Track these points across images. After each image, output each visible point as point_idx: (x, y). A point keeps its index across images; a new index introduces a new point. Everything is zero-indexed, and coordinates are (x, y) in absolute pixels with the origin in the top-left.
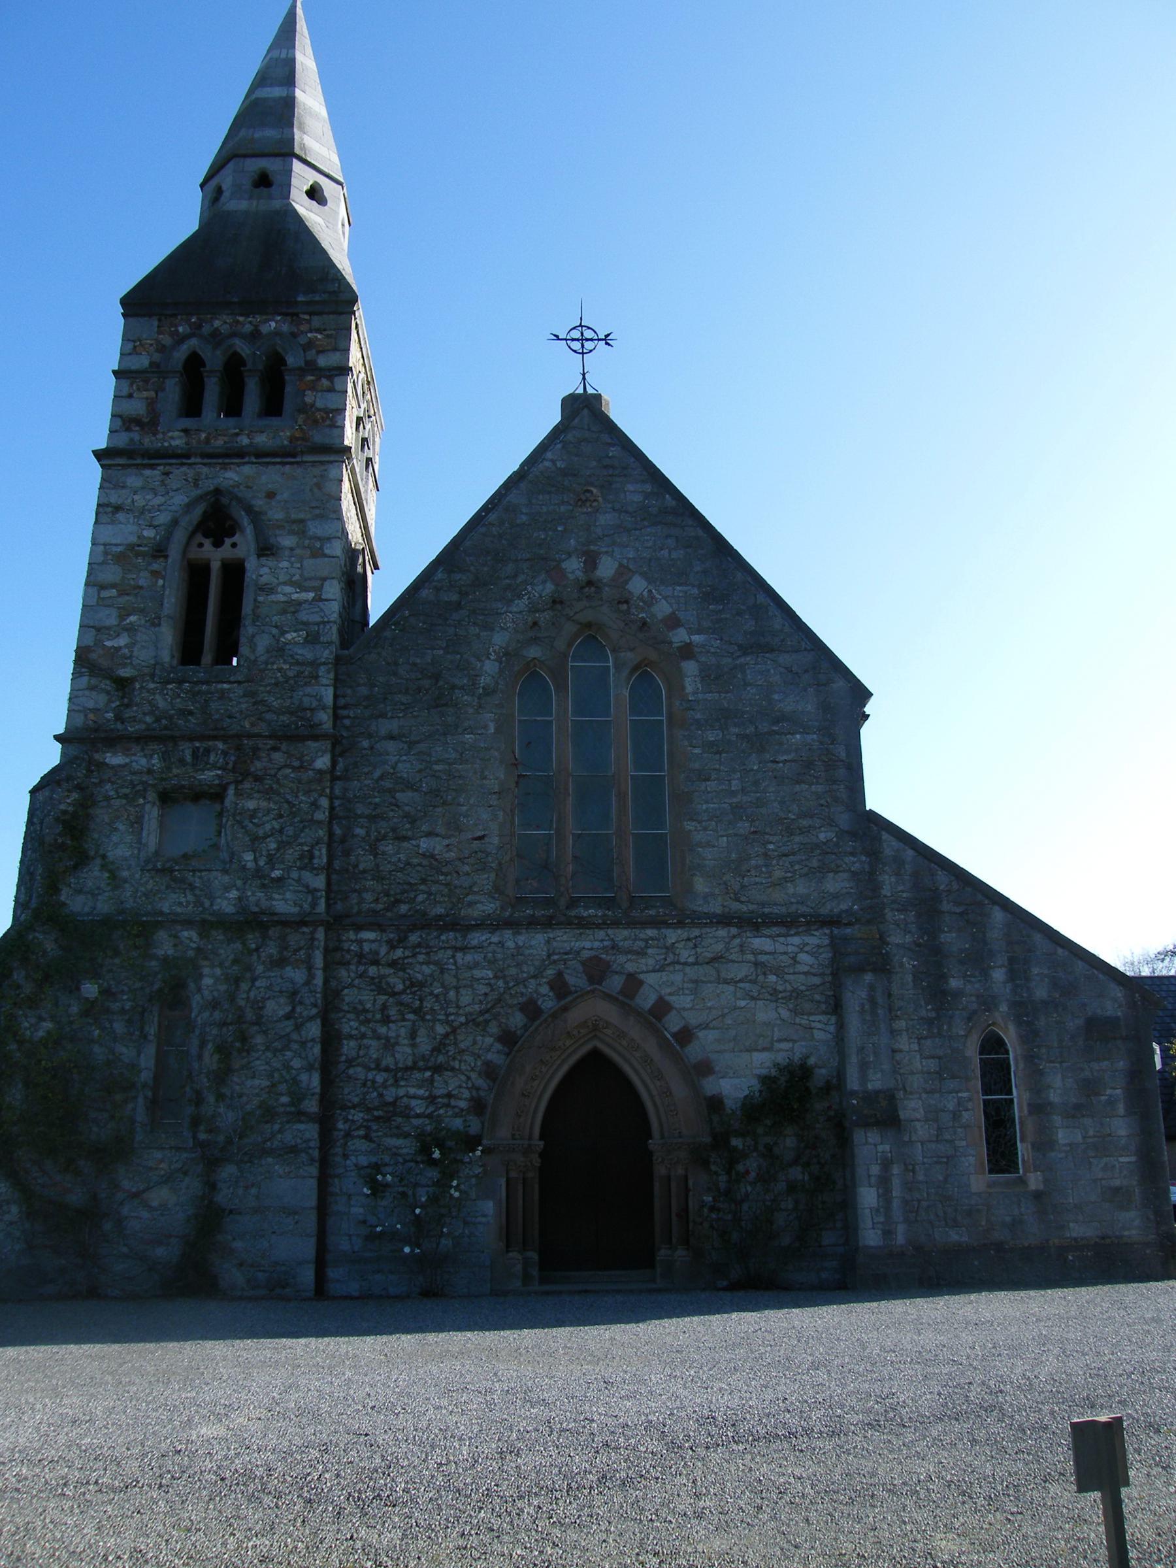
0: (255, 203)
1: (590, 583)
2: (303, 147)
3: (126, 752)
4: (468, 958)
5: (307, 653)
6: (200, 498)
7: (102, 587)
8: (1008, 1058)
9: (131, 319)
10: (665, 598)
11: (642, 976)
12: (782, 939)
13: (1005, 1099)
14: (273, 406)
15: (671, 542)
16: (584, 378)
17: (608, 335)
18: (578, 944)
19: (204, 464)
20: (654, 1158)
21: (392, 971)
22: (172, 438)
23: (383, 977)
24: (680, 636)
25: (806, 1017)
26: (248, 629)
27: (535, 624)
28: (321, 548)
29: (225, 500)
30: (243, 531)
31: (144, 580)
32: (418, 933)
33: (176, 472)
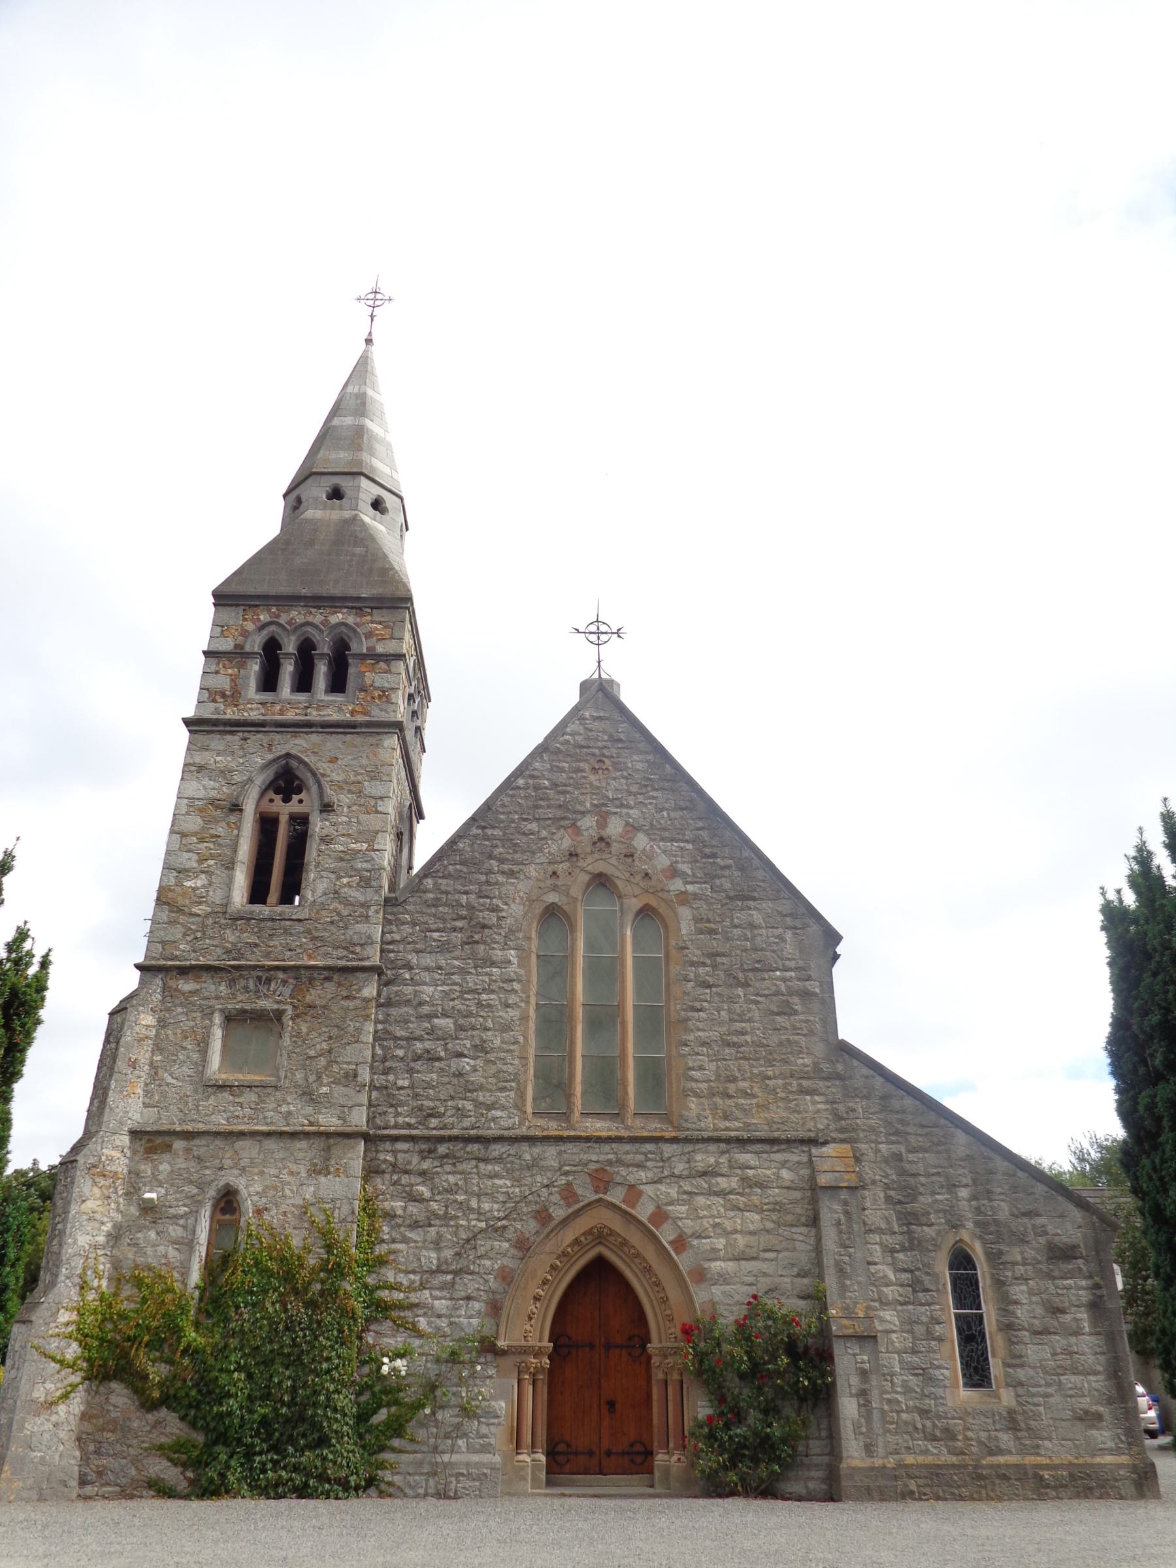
0: (328, 512)
1: (601, 839)
2: (373, 469)
3: (197, 979)
4: (490, 1167)
5: (357, 895)
6: (274, 760)
7: (183, 835)
8: (976, 1274)
9: (220, 608)
10: (664, 852)
11: (642, 1187)
12: (765, 1156)
13: (976, 1314)
14: (338, 684)
16: (599, 666)
18: (586, 1156)
19: (277, 732)
20: (653, 1361)
21: (422, 1180)
22: (251, 709)
23: (412, 1185)
24: (677, 885)
25: (788, 1229)
26: (310, 875)
27: (554, 873)
28: (375, 806)
29: (294, 764)
30: (308, 790)
31: (220, 830)
32: (446, 1145)
33: (253, 738)
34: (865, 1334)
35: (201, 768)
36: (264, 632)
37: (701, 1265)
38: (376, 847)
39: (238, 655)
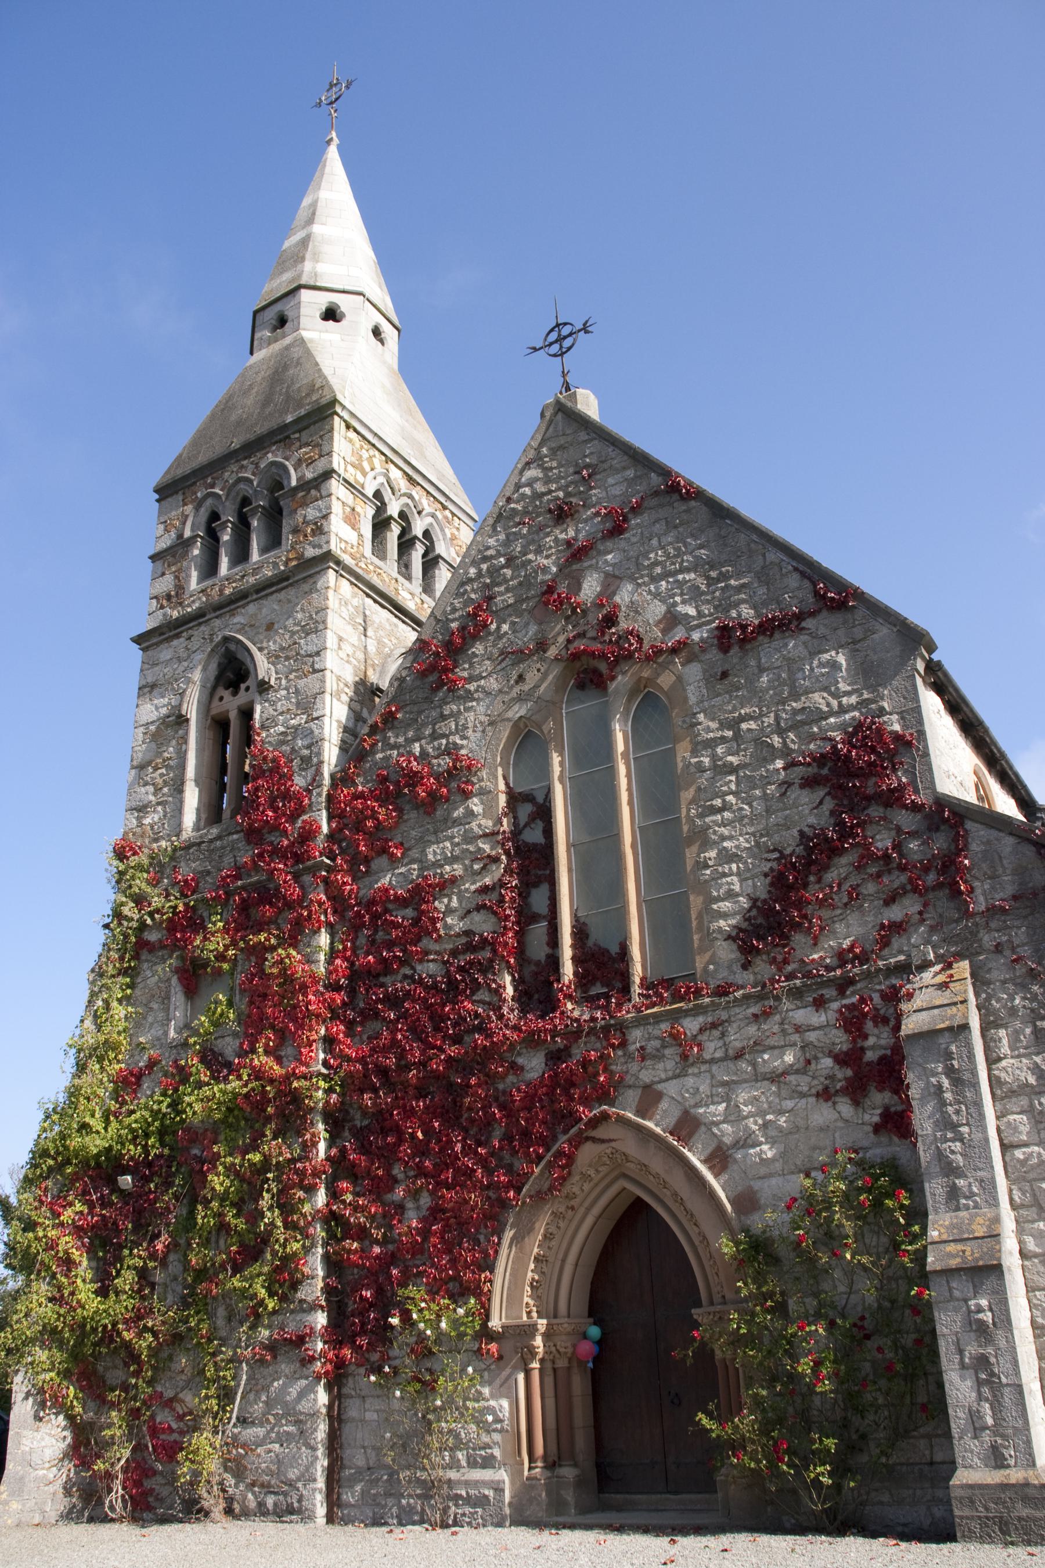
11: (659, 1087)
15: (658, 528)
17: (587, 322)
19: (217, 617)
29: (232, 647)
34: (981, 1263)
35: (153, 686)
36: (203, 510)
37: (751, 1187)
38: (315, 715)
39: (178, 549)
